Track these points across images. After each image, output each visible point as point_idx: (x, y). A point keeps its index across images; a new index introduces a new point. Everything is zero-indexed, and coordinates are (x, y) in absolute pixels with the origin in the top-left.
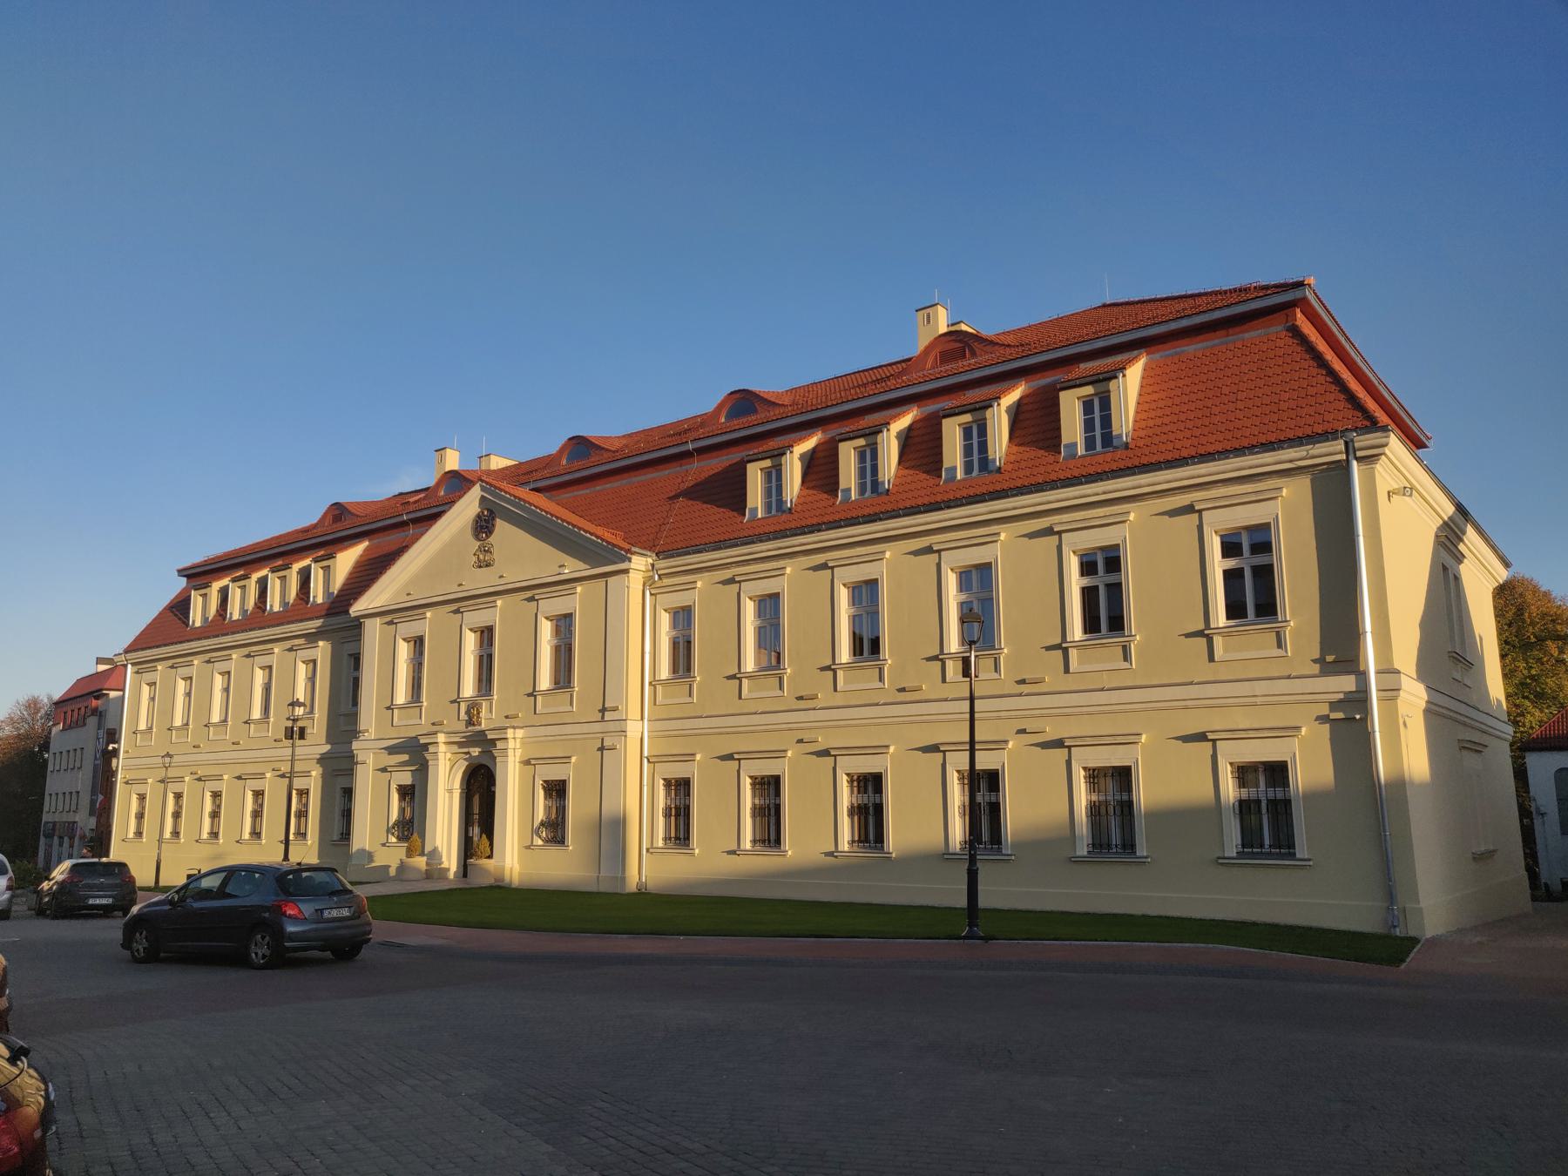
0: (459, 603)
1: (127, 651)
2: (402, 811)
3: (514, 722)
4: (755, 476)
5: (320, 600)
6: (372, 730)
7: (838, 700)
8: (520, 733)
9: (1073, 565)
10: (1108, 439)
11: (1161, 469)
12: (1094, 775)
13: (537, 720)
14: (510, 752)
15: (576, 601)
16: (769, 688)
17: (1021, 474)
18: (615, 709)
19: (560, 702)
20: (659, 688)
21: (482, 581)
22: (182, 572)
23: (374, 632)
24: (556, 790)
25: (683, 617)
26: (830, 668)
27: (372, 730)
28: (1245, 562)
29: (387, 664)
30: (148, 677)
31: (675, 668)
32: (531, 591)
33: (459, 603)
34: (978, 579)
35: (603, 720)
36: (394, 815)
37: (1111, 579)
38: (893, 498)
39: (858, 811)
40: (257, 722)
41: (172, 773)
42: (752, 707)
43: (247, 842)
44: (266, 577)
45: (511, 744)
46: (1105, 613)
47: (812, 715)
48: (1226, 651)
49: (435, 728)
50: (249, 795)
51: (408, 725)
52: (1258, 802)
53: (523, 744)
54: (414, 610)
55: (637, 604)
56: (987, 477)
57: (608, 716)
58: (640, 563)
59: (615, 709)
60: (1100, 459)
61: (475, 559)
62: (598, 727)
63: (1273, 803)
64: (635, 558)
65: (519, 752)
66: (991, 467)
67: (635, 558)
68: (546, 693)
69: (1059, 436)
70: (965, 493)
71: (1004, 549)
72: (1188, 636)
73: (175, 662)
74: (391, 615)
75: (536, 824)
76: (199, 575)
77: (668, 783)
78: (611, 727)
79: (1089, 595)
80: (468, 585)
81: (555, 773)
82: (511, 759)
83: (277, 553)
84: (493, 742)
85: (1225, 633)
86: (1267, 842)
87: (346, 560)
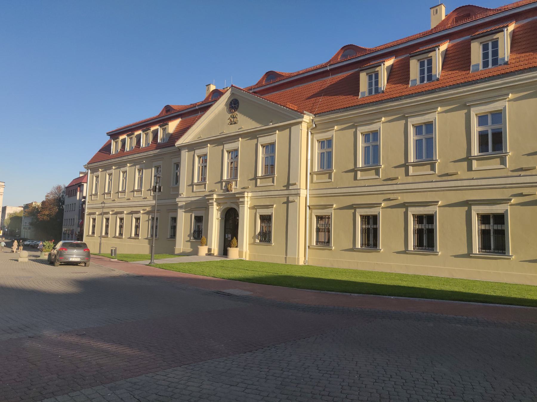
0: (220, 141)
1: (88, 164)
2: (262, 227)
3: (246, 190)
4: (363, 78)
5: (128, 150)
6: (185, 193)
7: (410, 179)
8: (250, 194)
9: (474, 121)
10: (377, 90)
11: (515, 75)
12: (484, 219)
13: (257, 189)
14: (246, 203)
15: (277, 137)
16: (371, 175)
17: (522, 63)
18: (295, 184)
19: (268, 182)
20: (315, 176)
21: (232, 130)
22: (108, 134)
23: (185, 155)
24: (266, 219)
25: (326, 144)
26: (255, 178)
27: (185, 193)
28: (489, 128)
29: (189, 165)
30: (96, 174)
31: (322, 165)
32: (253, 135)
33: (220, 141)
34: (372, 137)
35: (288, 189)
36: (258, 230)
37: (429, 136)
38: (387, 94)
39: (419, 233)
40: (137, 191)
41: (105, 210)
42: (362, 183)
43: (358, 250)
44: (158, 130)
45: (246, 199)
46: (426, 149)
47: (395, 187)
48: (413, 171)
49: (243, 190)
50: (134, 220)
51: (199, 192)
52: (490, 230)
53: (251, 199)
54: (201, 144)
55: (304, 140)
56: (496, 68)
57: (291, 187)
58: (307, 118)
59: (295, 184)
60: (373, 97)
61: (229, 121)
62: (286, 192)
63: (496, 232)
64: (305, 116)
65: (249, 203)
66: (379, 91)
67: (305, 116)
68: (261, 178)
69: (470, 62)
70: (413, 92)
71: (437, 116)
72: (396, 167)
73: (107, 168)
74: (191, 147)
75: (257, 233)
76: (114, 135)
77: (362, 217)
78: (293, 192)
79: (418, 143)
80: (226, 132)
81: (265, 212)
82: (246, 205)
83: (145, 126)
84: (238, 198)
85: (478, 159)
86: (492, 247)
87: (173, 126)
